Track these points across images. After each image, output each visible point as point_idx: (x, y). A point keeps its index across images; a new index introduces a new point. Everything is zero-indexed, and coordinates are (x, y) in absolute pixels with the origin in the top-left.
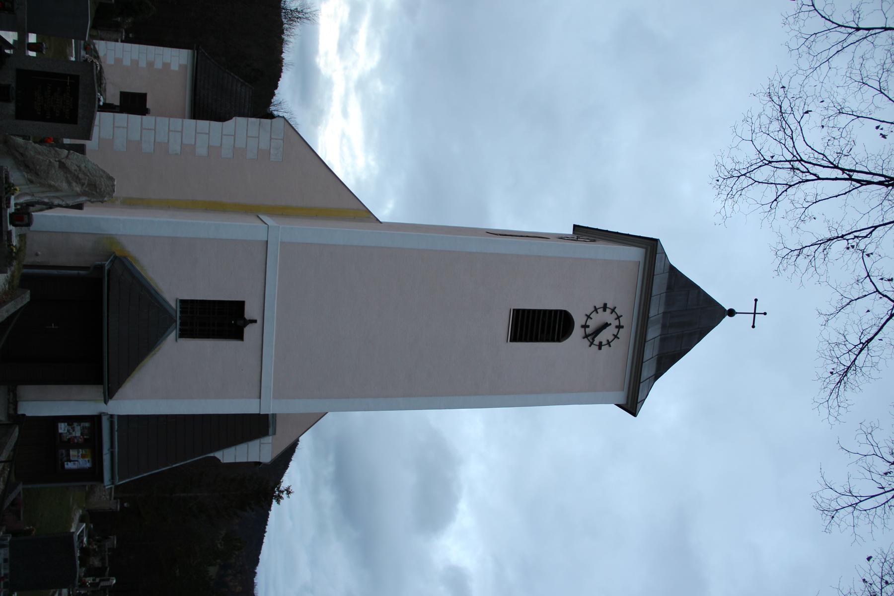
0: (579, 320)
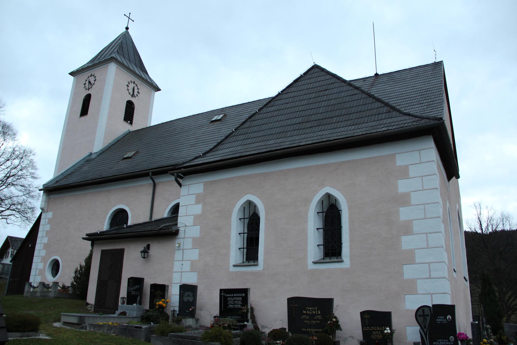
0: (130, 98)
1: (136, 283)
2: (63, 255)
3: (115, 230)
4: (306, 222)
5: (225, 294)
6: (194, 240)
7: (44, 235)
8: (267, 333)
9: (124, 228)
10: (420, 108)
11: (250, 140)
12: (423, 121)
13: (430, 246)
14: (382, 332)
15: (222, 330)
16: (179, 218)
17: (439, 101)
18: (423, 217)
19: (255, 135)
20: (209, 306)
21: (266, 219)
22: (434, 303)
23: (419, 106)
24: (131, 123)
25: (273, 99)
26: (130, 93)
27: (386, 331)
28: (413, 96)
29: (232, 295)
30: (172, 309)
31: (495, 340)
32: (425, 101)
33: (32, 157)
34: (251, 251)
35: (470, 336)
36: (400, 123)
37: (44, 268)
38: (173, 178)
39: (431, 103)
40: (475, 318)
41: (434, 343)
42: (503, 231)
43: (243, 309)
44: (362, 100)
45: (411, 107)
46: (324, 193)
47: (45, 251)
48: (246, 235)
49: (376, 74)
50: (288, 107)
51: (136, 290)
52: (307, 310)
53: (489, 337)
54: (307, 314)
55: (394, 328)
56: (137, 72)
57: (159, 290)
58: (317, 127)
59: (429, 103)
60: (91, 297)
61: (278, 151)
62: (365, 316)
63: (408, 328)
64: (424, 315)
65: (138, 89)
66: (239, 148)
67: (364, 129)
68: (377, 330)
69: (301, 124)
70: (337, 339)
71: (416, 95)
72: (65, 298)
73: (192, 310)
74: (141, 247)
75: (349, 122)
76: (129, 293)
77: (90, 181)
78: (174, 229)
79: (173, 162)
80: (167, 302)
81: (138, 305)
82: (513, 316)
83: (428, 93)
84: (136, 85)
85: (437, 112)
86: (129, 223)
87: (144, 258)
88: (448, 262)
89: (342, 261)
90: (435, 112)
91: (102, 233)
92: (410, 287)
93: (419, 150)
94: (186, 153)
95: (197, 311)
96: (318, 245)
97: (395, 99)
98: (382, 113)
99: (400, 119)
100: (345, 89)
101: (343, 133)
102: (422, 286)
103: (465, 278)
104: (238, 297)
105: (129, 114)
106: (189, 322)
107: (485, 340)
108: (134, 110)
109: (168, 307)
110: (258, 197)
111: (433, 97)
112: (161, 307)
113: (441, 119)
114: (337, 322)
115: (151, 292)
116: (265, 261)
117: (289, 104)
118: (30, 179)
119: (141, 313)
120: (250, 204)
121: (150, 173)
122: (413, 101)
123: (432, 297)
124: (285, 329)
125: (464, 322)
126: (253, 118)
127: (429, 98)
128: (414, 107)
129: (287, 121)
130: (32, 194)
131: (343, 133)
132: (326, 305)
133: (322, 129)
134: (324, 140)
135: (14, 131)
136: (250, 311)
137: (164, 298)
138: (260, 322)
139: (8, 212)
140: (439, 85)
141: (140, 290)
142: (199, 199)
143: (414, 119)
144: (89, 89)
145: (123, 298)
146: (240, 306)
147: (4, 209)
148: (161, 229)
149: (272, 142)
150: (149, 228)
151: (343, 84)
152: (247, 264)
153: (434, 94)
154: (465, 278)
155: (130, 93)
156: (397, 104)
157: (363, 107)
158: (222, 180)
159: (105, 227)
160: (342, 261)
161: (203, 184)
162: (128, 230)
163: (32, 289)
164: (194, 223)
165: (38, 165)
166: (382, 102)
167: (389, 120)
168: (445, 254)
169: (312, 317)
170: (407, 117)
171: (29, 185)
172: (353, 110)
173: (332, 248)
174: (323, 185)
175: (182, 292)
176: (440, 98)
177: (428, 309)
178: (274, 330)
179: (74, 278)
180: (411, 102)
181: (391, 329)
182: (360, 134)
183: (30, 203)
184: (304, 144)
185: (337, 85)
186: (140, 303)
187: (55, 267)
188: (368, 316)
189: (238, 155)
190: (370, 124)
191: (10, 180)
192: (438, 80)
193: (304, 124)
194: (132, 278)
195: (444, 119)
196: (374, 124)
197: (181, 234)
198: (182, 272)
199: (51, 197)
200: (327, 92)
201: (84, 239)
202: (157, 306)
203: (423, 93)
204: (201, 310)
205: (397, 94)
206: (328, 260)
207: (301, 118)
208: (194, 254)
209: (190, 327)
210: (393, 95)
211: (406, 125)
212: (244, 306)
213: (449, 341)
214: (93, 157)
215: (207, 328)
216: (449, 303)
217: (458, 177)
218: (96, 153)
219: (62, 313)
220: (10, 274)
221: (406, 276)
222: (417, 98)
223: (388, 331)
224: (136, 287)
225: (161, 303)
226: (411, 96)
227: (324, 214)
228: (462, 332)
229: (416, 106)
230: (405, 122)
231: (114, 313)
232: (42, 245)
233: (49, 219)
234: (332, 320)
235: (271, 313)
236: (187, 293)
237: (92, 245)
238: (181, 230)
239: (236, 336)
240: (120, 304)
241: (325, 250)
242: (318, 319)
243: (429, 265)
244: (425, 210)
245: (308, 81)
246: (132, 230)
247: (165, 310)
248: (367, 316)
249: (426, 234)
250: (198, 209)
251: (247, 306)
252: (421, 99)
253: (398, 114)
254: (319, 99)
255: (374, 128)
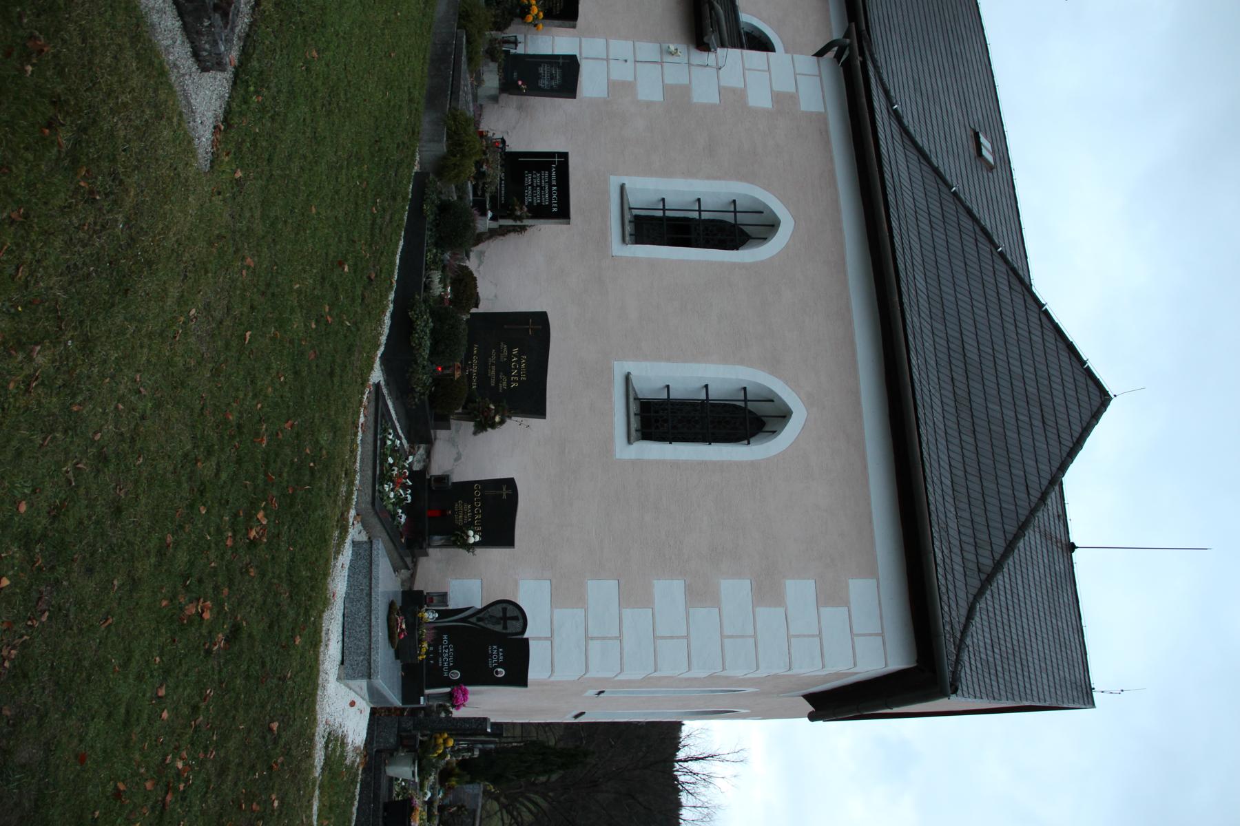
4: (724, 360)
5: (556, 165)
6: (686, 90)
8: (468, 263)
10: (982, 644)
11: (928, 229)
12: (952, 648)
13: (659, 642)
14: (470, 525)
15: (474, 158)
16: (737, 51)
17: (995, 689)
18: (726, 633)
19: (940, 242)
20: (529, 126)
21: (733, 266)
22: (531, 642)
23: (988, 641)
25: (1026, 286)
27: (471, 533)
28: (1014, 631)
29: (554, 183)
30: (520, 38)
31: (448, 763)
32: (997, 657)
34: (655, 227)
35: (456, 714)
36: (952, 595)
38: (837, 35)
39: (993, 671)
40: (498, 726)
41: (445, 637)
42: (679, 805)
43: (521, 209)
44: (1013, 508)
45: (986, 623)
46: (791, 405)
48: (695, 215)
49: (1072, 547)
50: (1006, 325)
52: (519, 356)
53: (454, 752)
54: (510, 357)
55: (478, 551)
58: (951, 396)
59: (992, 665)
61: (897, 299)
62: (504, 488)
63: (478, 582)
64: (505, 619)
66: (909, 201)
67: (941, 508)
68: (473, 517)
69: (961, 358)
70: (453, 422)
71: (1015, 636)
73: (519, 88)
75: (961, 474)
78: (712, 39)
79: (877, 33)
80: (535, 25)
82: (496, 806)
83: (1019, 666)
85: (970, 683)
88: (620, 681)
89: (629, 442)
90: (969, 678)
92: (568, 593)
93: (882, 635)
94: (898, 67)
95: (515, 97)
96: (668, 387)
97: (1008, 586)
98: (977, 554)
99: (962, 594)
100: (1044, 467)
101: (934, 456)
102: (570, 619)
103: (583, 713)
104: (551, 196)
106: (491, 80)
107: (451, 743)
109: (523, 28)
110: (787, 246)
111: (1007, 678)
113: (955, 691)
114: (493, 426)
116: (636, 261)
117: (1013, 328)
120: (772, 226)
122: (1000, 630)
123: (546, 638)
124: (477, 306)
125: (489, 703)
126: (982, 239)
127: (1006, 666)
128: (987, 630)
129: (971, 322)
131: (934, 456)
132: (532, 401)
133: (946, 408)
134: (920, 410)
136: (519, 223)
137: (546, 17)
138: (492, 248)
140: (1035, 693)
142: (785, 102)
143: (958, 628)
146: (528, 199)
148: (712, 8)
149: (921, 284)
151: (1056, 464)
152: (628, 217)
153: (1014, 681)
154: (583, 713)
156: (995, 590)
157: (997, 509)
158: (832, 159)
160: (629, 442)
166: (1005, 556)
167: (958, 569)
168: (638, 675)
169: (505, 367)
170: (964, 612)
172: (990, 486)
173: (661, 419)
174: (810, 401)
175: (561, 61)
176: (1003, 693)
177: (519, 630)
178: (475, 279)
180: (999, 624)
181: (475, 544)
182: (931, 498)
184: (914, 362)
185: (1055, 450)
188: (504, 497)
189: (891, 198)
190: (953, 524)
192: (1047, 693)
193: (962, 365)
195: (953, 697)
196: (953, 532)
197: (699, 57)
198: (607, 60)
200: (1037, 423)
203: (1017, 654)
204: (520, 108)
205: (1021, 594)
206: (634, 408)
207: (976, 358)
208: (649, 90)
209: (479, 81)
210: (1020, 582)
211: (946, 609)
212: (529, 211)
213: (450, 669)
215: (477, 124)
216: (532, 675)
217: (812, 717)
221: (592, 586)
222: (1008, 639)
223: (473, 538)
225: (535, 10)
226: (1013, 625)
227: (742, 404)
228: (470, 697)
229: (987, 635)
230: (954, 606)
234: (497, 413)
235: (511, 273)
236: (558, 73)
238: (710, 58)
239: (461, 190)
241: (656, 404)
242: (498, 381)
243: (616, 638)
244: (742, 637)
245: (1068, 379)
247: (517, 20)
248: (505, 492)
249: (687, 637)
250: (760, 98)
251: (528, 218)
252: (1003, 649)
253: (974, 591)
254: (1021, 403)
255: (943, 533)
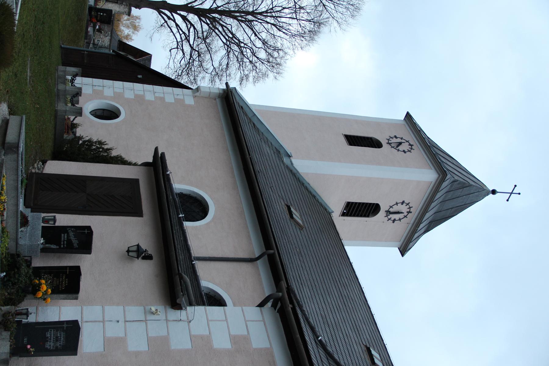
0: (384, 208)
1: (83, 241)
2: (126, 124)
3: (174, 200)
6: (165, 340)
7: (157, 95)
9: (178, 214)
16: (202, 308)
24: (343, 214)
26: (391, 207)
33: (271, 75)
37: (106, 98)
47: (132, 97)
51: (69, 241)
56: (428, 215)
57: (68, 283)
60: (55, 167)
65: (400, 220)
72: (55, 128)
74: (147, 245)
76: (64, 229)
77: (248, 156)
78: (183, 300)
80: (45, 299)
81: (42, 246)
84: (405, 217)
86: (187, 224)
87: (128, 251)
91: (167, 179)
105: (355, 210)
108: (365, 216)
109: (35, 302)
112: (35, 289)
115: (66, 267)
118: (239, 75)
119: (25, 252)
121: (272, 251)
130: (217, 80)
135: (308, 47)
137: (53, 292)
139: (187, 49)
141: (70, 249)
142: (240, 342)
144: (390, 144)
145: (54, 220)
147: (192, 43)
148: (181, 278)
150: (181, 257)
155: (391, 207)
159: (179, 185)
161: (269, 346)
162: (175, 221)
163: (69, 78)
164: (195, 336)
165: (260, 84)
171: (230, 75)
179: (90, 141)
183: (203, 78)
186: (44, 250)
187: (108, 114)
191: (235, 48)
194: (91, 232)
197: (174, 314)
199: (218, 101)
201: (156, 150)
202: (37, 281)
208: (137, 342)
214: (285, 160)
218: (292, 164)
219: (24, 117)
220: (97, 51)
224: (75, 242)
225: (44, 287)
231: (26, 205)
232: (142, 93)
233: (183, 100)
236: (62, 336)
237: (146, 164)
238: (182, 314)
240: (43, 215)
246: (176, 227)
250: (221, 341)
